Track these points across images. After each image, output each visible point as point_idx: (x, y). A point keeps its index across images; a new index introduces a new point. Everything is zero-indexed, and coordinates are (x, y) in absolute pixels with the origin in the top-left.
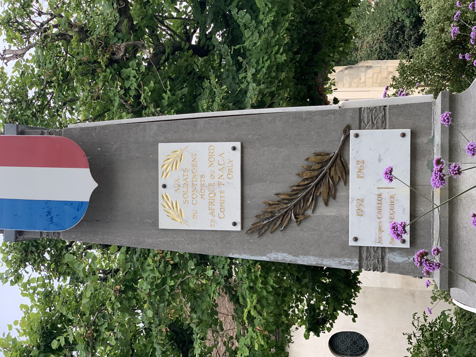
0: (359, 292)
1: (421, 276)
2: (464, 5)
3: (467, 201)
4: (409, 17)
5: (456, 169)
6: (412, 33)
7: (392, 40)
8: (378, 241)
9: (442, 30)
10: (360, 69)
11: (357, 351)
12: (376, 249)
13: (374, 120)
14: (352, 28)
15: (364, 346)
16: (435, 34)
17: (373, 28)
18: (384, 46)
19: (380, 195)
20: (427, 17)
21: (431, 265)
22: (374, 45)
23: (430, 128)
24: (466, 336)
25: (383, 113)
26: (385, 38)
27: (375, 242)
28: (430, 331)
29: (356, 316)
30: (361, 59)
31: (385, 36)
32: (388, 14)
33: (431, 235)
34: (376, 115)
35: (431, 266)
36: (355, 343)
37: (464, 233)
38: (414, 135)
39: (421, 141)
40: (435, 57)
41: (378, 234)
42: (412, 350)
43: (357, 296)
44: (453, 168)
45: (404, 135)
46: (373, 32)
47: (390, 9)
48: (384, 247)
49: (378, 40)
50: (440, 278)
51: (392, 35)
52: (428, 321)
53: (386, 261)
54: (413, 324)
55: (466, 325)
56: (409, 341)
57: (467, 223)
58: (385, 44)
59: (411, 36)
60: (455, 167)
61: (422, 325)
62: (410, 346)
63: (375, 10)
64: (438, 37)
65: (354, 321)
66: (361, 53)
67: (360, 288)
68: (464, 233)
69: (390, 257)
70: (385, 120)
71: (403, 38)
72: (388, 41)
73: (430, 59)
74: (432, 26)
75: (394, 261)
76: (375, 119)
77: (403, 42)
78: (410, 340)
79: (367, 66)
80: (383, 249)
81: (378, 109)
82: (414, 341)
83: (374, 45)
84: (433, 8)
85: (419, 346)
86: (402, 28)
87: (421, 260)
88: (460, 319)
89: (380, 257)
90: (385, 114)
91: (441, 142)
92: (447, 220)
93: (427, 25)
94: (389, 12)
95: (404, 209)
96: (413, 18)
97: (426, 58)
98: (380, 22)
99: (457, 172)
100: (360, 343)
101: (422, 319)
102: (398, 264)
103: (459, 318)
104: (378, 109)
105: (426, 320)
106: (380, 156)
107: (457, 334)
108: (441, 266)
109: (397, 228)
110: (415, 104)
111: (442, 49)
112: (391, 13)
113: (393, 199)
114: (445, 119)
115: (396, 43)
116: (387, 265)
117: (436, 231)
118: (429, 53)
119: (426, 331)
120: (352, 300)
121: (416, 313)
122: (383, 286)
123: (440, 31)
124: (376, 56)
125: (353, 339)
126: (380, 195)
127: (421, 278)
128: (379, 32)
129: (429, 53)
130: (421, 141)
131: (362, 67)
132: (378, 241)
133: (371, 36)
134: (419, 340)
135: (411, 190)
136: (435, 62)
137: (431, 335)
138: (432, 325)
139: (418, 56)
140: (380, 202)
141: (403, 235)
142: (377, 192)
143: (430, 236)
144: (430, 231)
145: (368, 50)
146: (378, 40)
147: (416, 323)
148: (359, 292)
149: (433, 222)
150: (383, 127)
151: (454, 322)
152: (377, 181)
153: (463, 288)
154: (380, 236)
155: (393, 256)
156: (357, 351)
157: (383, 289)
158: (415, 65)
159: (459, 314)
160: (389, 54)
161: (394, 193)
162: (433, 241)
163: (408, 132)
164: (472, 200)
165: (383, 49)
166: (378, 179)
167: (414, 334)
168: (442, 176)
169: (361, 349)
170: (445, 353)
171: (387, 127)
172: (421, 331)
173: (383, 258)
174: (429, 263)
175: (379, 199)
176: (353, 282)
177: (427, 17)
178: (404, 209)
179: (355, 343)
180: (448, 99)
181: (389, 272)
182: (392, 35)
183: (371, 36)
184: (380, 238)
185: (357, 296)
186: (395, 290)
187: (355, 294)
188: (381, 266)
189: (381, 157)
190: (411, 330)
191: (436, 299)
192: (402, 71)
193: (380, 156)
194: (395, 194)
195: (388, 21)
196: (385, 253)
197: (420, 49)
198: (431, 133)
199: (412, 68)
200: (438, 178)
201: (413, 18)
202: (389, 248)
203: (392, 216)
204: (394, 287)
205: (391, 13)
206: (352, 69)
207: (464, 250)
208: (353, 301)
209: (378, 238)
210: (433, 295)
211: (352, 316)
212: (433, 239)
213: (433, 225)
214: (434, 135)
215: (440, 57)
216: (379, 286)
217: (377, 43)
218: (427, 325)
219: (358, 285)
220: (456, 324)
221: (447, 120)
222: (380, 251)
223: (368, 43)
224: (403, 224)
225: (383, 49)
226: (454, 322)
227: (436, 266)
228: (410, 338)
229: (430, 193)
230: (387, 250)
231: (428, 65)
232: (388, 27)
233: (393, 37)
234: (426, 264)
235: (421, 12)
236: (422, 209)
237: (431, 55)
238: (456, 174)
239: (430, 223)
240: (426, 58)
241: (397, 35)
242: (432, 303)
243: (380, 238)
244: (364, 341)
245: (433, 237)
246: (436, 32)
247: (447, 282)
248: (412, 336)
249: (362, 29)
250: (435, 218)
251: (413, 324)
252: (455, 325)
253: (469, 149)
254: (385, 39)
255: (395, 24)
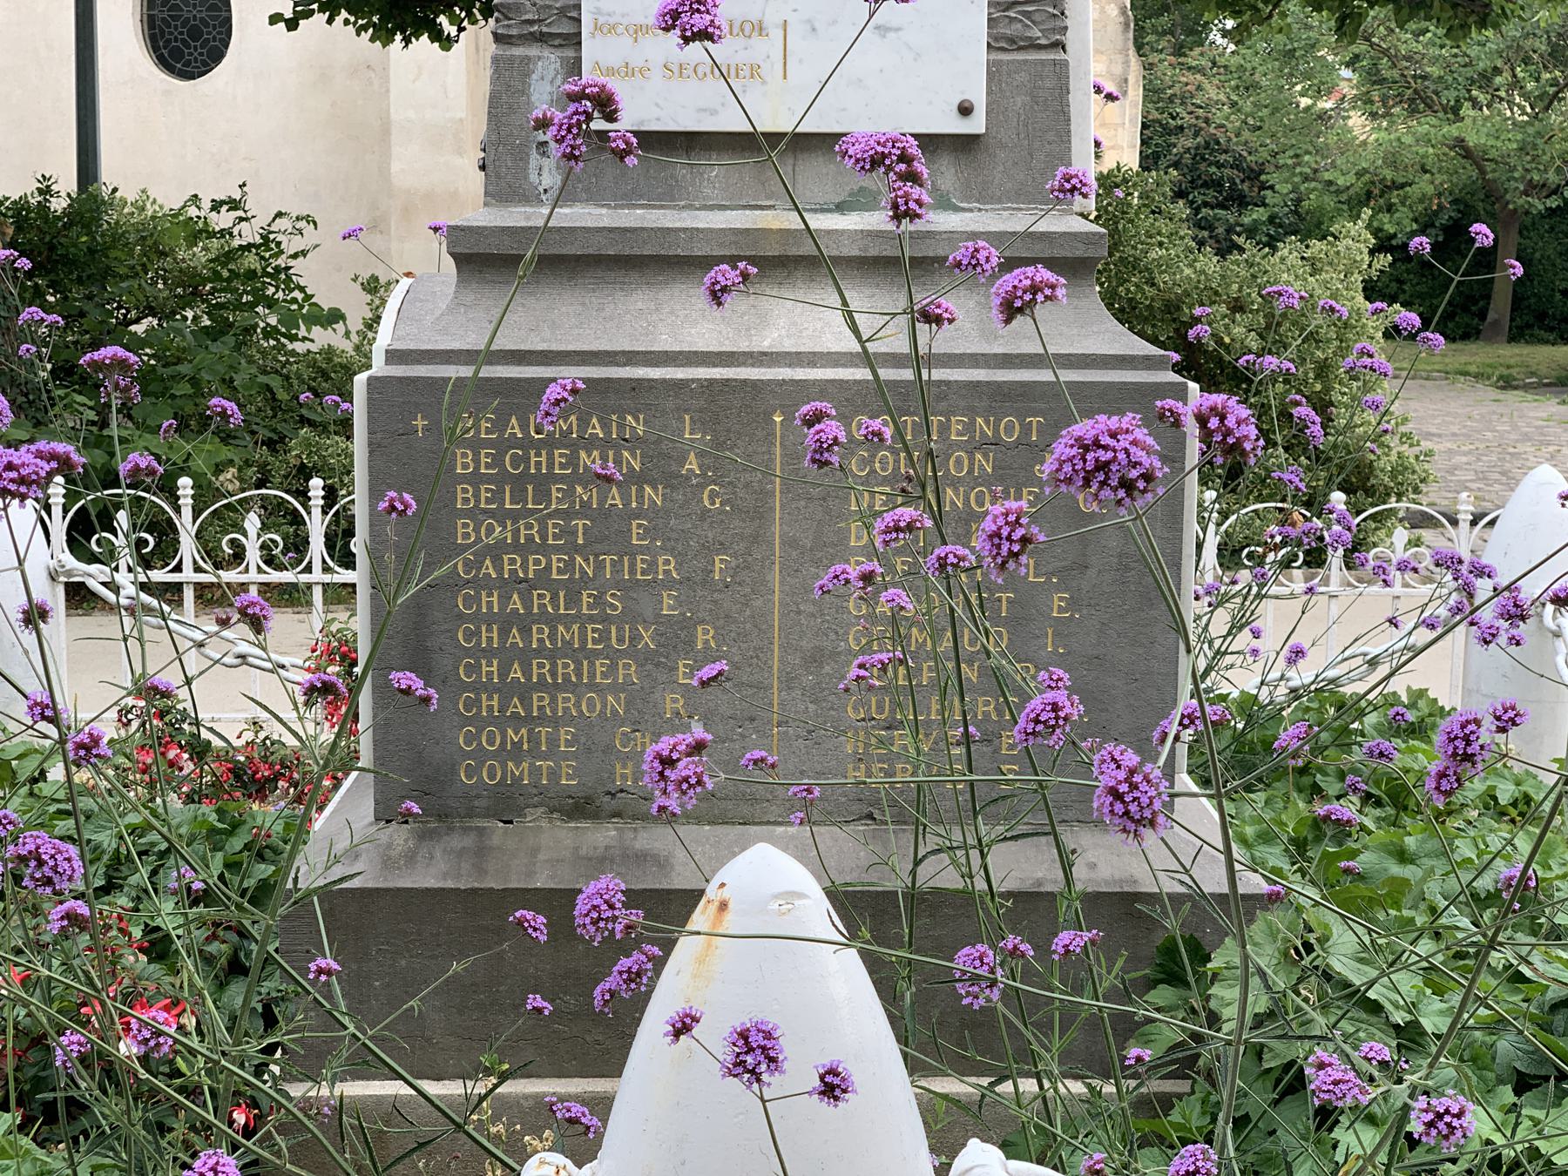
0: (372, 40)
1: (490, 168)
2: (1311, 375)
3: (744, 314)
4: (1271, 219)
5: (912, 205)
6: (1220, 230)
7: (1203, 166)
8: (601, 20)
9: (1238, 306)
10: (1119, 58)
11: (169, 41)
12: (574, 14)
13: (1020, 8)
14: (1270, 16)
15: (188, 64)
16: (1229, 285)
17: (1248, 106)
18: (1185, 142)
19: (760, 29)
20: (1283, 259)
21: (575, 131)
22: (1191, 108)
23: (984, 196)
24: (262, 379)
25: (1043, 42)
26: (1211, 145)
27: (598, 11)
28: (264, 269)
29: (292, 25)
30: (1148, 67)
31: (1218, 143)
32: (1291, 153)
33: (628, 199)
34: (1037, 17)
35: (569, 131)
36: (195, 34)
37: (640, 305)
38: (964, 144)
39: (943, 169)
40: (1153, 285)
41: (625, 22)
42: (193, 212)
43: (358, 34)
44: (915, 197)
45: (965, 110)
46: (1234, 104)
47: (1307, 158)
48: (580, 43)
49: (1207, 121)
50: (485, 228)
51: (1219, 166)
52: (291, 263)
53: (533, 51)
54: (279, 215)
55: (295, 382)
56: (222, 203)
57: (672, 312)
58: (1189, 143)
59: (1211, 228)
60: (919, 203)
61: (279, 244)
62: (206, 204)
63: (1308, 109)
64: (1216, 293)
65: (275, 19)
66: (1166, 65)
67: (387, 41)
68: (640, 305)
69: (548, 62)
70: (1020, 48)
71: (1206, 204)
72: (1198, 156)
73: (1147, 269)
74: (1254, 277)
75: (534, 76)
76: (1024, 13)
77: (1192, 202)
78: (225, 207)
79: (1126, 81)
80: (575, 40)
81: (1059, 23)
82: (223, 220)
83: (1191, 108)
84: (1311, 279)
85: (212, 235)
86: (1242, 202)
87: (588, 97)
88: (313, 364)
89: (545, 29)
90: (1041, 47)
91: (940, 233)
92: (679, 252)
93: (1257, 259)
94: (1297, 156)
95: (714, 112)
96: (1268, 235)
97: (1152, 255)
98: (1266, 128)
99: (903, 208)
100: (196, 52)
101: (295, 244)
102: (524, 91)
103: (315, 361)
104: (1059, 23)
105: (295, 256)
106: (898, 29)
107: (263, 353)
108: (573, 163)
109: (698, 11)
110: (1070, 149)
111: (1178, 308)
112: (1290, 162)
113: (748, 73)
114: (1074, 181)
115: (1192, 182)
116: (518, 51)
117: (643, 218)
118: (1168, 265)
119: (262, 258)
120: (344, 14)
121: (315, 223)
122: (394, 131)
123: (1236, 300)
124: (1155, 115)
125: (207, 25)
126: (760, 29)
127: (483, 168)
128: (1235, 122)
129: (1168, 265)
130: (943, 169)
131: (1127, 63)
132: (601, 20)
133: (1222, 97)
134: (231, 234)
135: (784, 135)
136: (1137, 285)
137: (251, 275)
138: (283, 276)
139: (1159, 234)
140: (735, 31)
141: (678, 31)
142: (772, 19)
143: (625, 196)
144: (641, 197)
145: (1177, 89)
146: (1207, 121)
147: (282, 224)
148: (372, 40)
149: (674, 207)
150: (996, 39)
151: (299, 347)
152: (809, 21)
153: (457, 303)
154: (620, 29)
155: (552, 73)
156: (169, 41)
157: (385, 131)
158: (1131, 221)
159: (329, 360)
160: (1156, 157)
161: (768, 79)
162: (609, 207)
163: (976, 125)
164: (748, 330)
165: (1173, 140)
166: (817, 25)
167: (246, 219)
168: (888, 162)
169: (177, 54)
170: (195, 318)
171: (992, 57)
172: (258, 240)
173: (542, 38)
174: (579, 123)
175: (748, 27)
176: (409, 19)
177: (1283, 259)
178: (714, 112)
179: (195, 34)
180: (1078, 253)
181: (496, 60)
182: (1219, 166)
183: (1222, 97)
184: (613, 28)
185: (358, 34)
186: (384, 172)
187: (364, 28)
188: (514, 32)
189: (891, 35)
190: (260, 209)
191: (369, 292)
192: (1118, 180)
193: (898, 29)
194: (764, 83)
195: (1265, 155)
196: (561, 45)
197: (1182, 238)
198: (968, 199)
199: (1124, 213)
200: (880, 149)
201: (1268, 235)
202: (579, 60)
203: (690, 71)
204: (395, 167)
205: (1290, 162)
206: (1120, 28)
207: (583, 304)
208: (339, 20)
209: (612, 21)
210: (382, 281)
211: (289, 14)
212: (615, 208)
213: (662, 207)
214: (964, 210)
215: (1153, 300)
216: (394, 116)
217: (1197, 118)
218: (281, 262)
219: (398, 37)
220: (293, 353)
221: (1068, 186)
222: (565, 28)
223: (1199, 88)
224: (717, 32)
225: (1173, 140)
226: (299, 347)
227: (573, 147)
228: (234, 205)
229: (768, 198)
230: (570, 53)
231: (1134, 265)
232: (1245, 154)
233: (1213, 169)
234: (576, 113)
235: (1301, 241)
236: (716, 172)
237: (1162, 272)
238: (895, 206)
239: (668, 197)
240: (1152, 255)
241: (1217, 184)
242: (355, 280)
243: (613, 28)
244: (205, 64)
245: (622, 207)
246: (1235, 287)
247: (475, 250)
248: (240, 213)
249: (1249, 66)
250: (685, 214)
251: (279, 215)
252: (290, 347)
253: (977, 250)
254: (1207, 144)
255: (1254, 175)
